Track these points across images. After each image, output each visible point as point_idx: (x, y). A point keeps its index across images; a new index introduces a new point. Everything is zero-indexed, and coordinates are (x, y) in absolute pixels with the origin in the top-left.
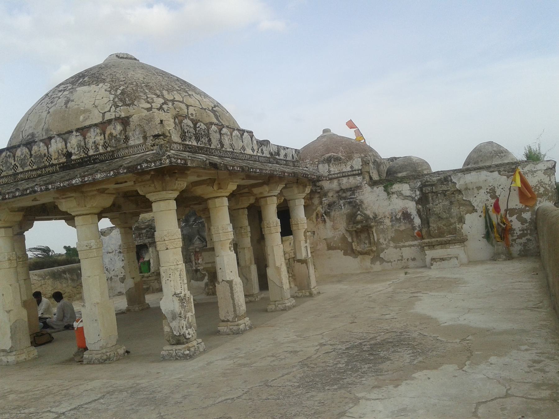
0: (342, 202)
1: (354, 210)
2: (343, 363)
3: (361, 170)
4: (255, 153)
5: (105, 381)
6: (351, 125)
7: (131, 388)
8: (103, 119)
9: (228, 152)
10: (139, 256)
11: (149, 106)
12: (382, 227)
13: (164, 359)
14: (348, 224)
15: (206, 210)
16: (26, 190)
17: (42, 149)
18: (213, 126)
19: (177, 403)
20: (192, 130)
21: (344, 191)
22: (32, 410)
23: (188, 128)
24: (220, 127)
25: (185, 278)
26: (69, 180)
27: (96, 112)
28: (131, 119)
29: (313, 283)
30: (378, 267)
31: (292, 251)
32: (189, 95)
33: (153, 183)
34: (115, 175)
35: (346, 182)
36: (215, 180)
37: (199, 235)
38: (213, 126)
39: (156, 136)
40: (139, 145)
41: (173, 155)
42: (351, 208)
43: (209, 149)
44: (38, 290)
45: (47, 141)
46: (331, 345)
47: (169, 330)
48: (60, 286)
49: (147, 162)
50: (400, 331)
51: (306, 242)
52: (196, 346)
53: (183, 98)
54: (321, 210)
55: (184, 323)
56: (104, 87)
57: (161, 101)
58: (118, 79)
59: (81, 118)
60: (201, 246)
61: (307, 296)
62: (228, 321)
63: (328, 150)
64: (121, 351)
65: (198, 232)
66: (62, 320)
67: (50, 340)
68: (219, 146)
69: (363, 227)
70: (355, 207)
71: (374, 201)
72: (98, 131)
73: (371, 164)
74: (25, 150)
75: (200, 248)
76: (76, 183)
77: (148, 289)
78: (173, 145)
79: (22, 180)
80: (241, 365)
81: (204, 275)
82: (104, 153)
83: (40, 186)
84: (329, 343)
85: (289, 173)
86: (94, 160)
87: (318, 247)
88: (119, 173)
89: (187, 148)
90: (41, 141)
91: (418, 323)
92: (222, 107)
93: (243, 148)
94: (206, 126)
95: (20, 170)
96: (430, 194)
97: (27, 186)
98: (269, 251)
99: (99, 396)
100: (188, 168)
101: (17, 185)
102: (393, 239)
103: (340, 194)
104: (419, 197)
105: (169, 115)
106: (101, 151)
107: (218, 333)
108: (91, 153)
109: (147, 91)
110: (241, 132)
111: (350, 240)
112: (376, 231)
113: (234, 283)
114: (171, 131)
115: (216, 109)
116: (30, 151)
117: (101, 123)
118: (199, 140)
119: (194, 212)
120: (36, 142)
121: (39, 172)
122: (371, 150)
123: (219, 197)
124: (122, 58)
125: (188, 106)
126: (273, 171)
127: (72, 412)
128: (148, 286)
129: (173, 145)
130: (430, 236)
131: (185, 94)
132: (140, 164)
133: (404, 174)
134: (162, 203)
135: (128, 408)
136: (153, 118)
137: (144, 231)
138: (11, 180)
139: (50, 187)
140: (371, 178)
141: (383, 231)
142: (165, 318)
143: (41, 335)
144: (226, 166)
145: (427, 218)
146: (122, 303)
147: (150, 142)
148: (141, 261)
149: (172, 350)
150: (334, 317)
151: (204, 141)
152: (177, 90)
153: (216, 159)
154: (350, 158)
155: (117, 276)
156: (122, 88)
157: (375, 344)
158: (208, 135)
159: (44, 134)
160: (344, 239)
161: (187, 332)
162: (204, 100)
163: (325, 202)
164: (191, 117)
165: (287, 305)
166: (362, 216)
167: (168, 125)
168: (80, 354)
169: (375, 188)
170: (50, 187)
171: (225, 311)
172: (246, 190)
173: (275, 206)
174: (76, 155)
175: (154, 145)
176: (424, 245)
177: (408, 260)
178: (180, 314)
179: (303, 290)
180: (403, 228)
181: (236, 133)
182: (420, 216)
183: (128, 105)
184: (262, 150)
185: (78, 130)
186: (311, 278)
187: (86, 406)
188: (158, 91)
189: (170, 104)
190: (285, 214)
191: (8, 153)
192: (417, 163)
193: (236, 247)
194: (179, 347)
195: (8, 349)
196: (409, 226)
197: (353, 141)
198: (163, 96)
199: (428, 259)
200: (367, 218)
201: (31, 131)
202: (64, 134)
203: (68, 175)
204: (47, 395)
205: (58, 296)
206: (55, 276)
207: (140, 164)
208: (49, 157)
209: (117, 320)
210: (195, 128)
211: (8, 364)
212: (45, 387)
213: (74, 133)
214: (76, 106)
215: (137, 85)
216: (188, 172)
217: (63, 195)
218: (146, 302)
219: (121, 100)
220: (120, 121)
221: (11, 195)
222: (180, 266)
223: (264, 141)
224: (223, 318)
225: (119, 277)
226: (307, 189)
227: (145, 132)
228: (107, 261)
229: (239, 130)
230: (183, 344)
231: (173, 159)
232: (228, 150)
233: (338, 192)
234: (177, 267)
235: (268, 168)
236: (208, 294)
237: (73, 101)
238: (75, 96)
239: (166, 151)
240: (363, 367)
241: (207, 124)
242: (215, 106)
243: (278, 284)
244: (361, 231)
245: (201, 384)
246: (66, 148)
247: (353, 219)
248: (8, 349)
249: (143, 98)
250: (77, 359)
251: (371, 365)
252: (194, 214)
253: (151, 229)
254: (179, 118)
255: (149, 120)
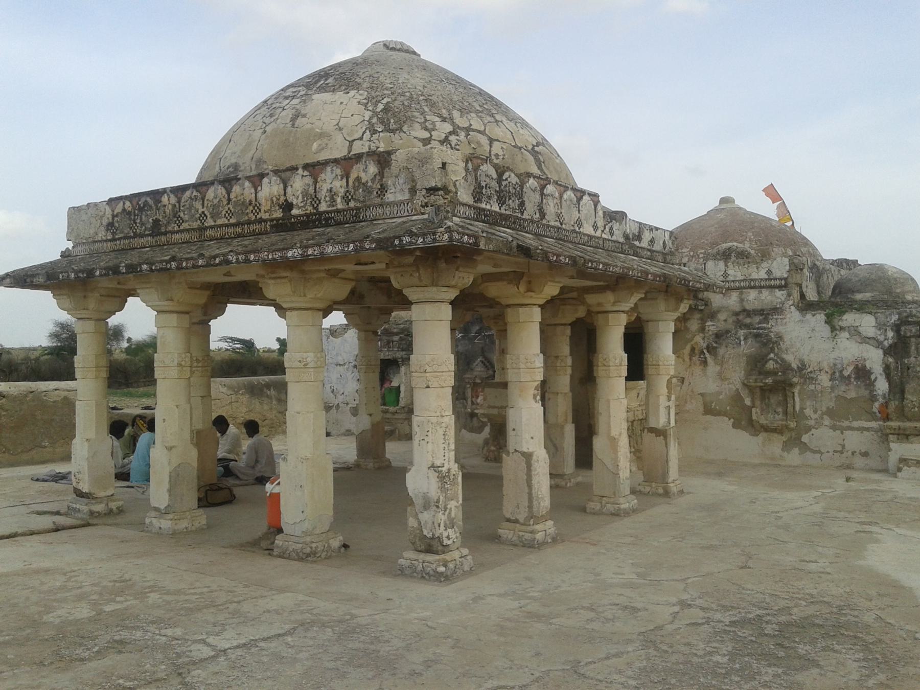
0: (742, 333)
1: (764, 350)
2: (724, 655)
3: (786, 279)
4: (598, 234)
5: (301, 597)
6: (771, 193)
7: (340, 621)
8: (349, 152)
9: (552, 227)
10: (384, 378)
11: (426, 135)
12: (812, 387)
13: (402, 573)
14: (748, 374)
15: (500, 318)
16: (215, 257)
17: (247, 192)
18: (531, 180)
19: (413, 673)
20: (494, 184)
21: (748, 313)
22: (178, 632)
23: (488, 180)
24: (542, 182)
25: (452, 440)
26: (284, 249)
27: (339, 139)
28: (393, 157)
29: (673, 473)
30: (794, 457)
31: (640, 409)
32: (497, 121)
33: (418, 270)
34: (356, 250)
35: (753, 298)
36: (523, 273)
37: (484, 357)
38: (531, 180)
39: (432, 190)
40: (402, 202)
41: (455, 228)
42: (757, 345)
43: (520, 219)
44: (220, 412)
45: (256, 179)
46: (702, 609)
47: (416, 525)
48: (258, 410)
49: (411, 234)
50: (838, 603)
51: (669, 400)
52: (458, 560)
53: (485, 125)
54: (702, 341)
55: (442, 517)
56: (358, 96)
57: (448, 127)
58: (382, 85)
59: (315, 146)
60: (484, 375)
61: (660, 495)
62: (516, 521)
63: (726, 235)
64: (336, 543)
65: (483, 351)
66: (253, 467)
67: (230, 500)
68: (538, 215)
69: (776, 383)
70: (765, 345)
71: (804, 338)
72: (338, 171)
73: (805, 270)
74: (221, 191)
75: (482, 379)
76: (293, 256)
77: (392, 433)
78: (458, 208)
79: (211, 240)
80: (532, 615)
81: (484, 425)
82: (344, 210)
83: (238, 254)
84: (698, 602)
85: (655, 275)
86: (327, 219)
87: (688, 407)
88: (362, 248)
89: (482, 215)
90: (248, 178)
91: (873, 592)
92: (550, 146)
93: (579, 223)
94: (517, 177)
95: (210, 222)
96: (913, 340)
97: (217, 252)
98: (601, 407)
99: (287, 627)
100: (480, 252)
101: (202, 247)
102: (830, 413)
103: (741, 317)
104: (890, 342)
105: (458, 154)
106: (340, 206)
107: (495, 538)
108: (323, 207)
109: (426, 109)
110: (579, 194)
111: (748, 402)
112: (799, 393)
113: (534, 458)
114: (457, 183)
115: (539, 150)
116: (229, 193)
117: (345, 159)
118: (504, 203)
119: (480, 331)
120: (240, 179)
121: (239, 230)
122: (806, 242)
123: (526, 305)
124: (393, 49)
125: (491, 141)
126: (628, 269)
127: (239, 652)
128: (392, 428)
129: (458, 208)
130: (902, 414)
131: (489, 119)
132: (399, 237)
133: (867, 296)
134: (428, 307)
135: (331, 665)
136: (431, 157)
137: (396, 338)
138: (194, 236)
139: (252, 257)
140: (802, 296)
141: (813, 395)
142: (412, 503)
143: (216, 490)
144: (545, 254)
145: (902, 383)
146: (348, 451)
147: (420, 199)
148: (386, 385)
149: (417, 560)
150: (708, 548)
151: (512, 205)
152: (477, 112)
153: (529, 240)
154: (765, 255)
155: (347, 404)
156: (385, 101)
157: (789, 624)
158: (520, 195)
159: (254, 167)
160: (737, 398)
161: (445, 534)
162: (521, 131)
163: (711, 328)
164: (495, 161)
165: (622, 506)
166: (777, 362)
167: (454, 172)
168: (268, 539)
169: (809, 316)
170: (252, 257)
171: (512, 502)
172: (574, 294)
173: (622, 330)
174: (299, 208)
175: (426, 205)
176: (888, 431)
177: (853, 453)
178: (438, 501)
179: (653, 483)
180: (852, 394)
181: (569, 194)
182: (888, 377)
183: (393, 131)
184: (611, 228)
185: (306, 167)
186: (670, 464)
187: (262, 644)
188: (444, 111)
189: (462, 134)
190: (636, 343)
191: (195, 193)
192: (895, 279)
193: (545, 391)
194: (430, 558)
195: (162, 507)
196: (866, 393)
197: (774, 223)
198: (452, 119)
199: (893, 458)
200: (786, 367)
201: (233, 161)
202: (284, 171)
203: (282, 241)
204: (207, 607)
205: (252, 428)
206: (254, 391)
207: (399, 237)
208: (257, 207)
209: (336, 480)
210: (500, 180)
211: (160, 533)
212: (206, 590)
213: (300, 171)
214: (309, 126)
215: (411, 97)
216: (479, 258)
217: (273, 272)
218: (387, 456)
219: (382, 121)
220: (376, 158)
221: (190, 264)
222: (446, 420)
223: (616, 212)
224: (508, 515)
225: (350, 406)
226: (682, 305)
227: (413, 181)
228: (334, 376)
229: (575, 190)
230: (437, 553)
231: (455, 234)
232: (552, 223)
233: (737, 314)
234: (441, 420)
235: (619, 264)
236: (487, 459)
237: (304, 116)
238: (308, 109)
239: (446, 218)
240: (763, 670)
241: (521, 174)
242: (538, 145)
243: (610, 467)
244: (771, 392)
245: (458, 640)
246: (285, 195)
247: (759, 365)
248: (162, 507)
249: (418, 120)
250: (264, 544)
251: (780, 671)
252: (480, 320)
253: (408, 335)
254: (473, 160)
255: (424, 161)
